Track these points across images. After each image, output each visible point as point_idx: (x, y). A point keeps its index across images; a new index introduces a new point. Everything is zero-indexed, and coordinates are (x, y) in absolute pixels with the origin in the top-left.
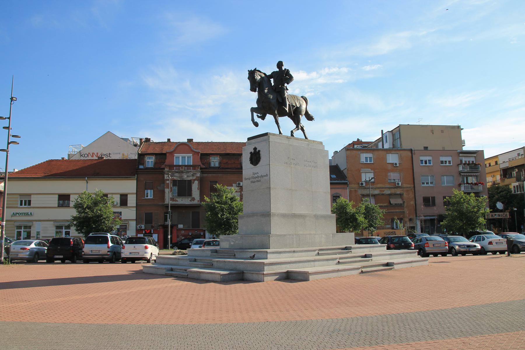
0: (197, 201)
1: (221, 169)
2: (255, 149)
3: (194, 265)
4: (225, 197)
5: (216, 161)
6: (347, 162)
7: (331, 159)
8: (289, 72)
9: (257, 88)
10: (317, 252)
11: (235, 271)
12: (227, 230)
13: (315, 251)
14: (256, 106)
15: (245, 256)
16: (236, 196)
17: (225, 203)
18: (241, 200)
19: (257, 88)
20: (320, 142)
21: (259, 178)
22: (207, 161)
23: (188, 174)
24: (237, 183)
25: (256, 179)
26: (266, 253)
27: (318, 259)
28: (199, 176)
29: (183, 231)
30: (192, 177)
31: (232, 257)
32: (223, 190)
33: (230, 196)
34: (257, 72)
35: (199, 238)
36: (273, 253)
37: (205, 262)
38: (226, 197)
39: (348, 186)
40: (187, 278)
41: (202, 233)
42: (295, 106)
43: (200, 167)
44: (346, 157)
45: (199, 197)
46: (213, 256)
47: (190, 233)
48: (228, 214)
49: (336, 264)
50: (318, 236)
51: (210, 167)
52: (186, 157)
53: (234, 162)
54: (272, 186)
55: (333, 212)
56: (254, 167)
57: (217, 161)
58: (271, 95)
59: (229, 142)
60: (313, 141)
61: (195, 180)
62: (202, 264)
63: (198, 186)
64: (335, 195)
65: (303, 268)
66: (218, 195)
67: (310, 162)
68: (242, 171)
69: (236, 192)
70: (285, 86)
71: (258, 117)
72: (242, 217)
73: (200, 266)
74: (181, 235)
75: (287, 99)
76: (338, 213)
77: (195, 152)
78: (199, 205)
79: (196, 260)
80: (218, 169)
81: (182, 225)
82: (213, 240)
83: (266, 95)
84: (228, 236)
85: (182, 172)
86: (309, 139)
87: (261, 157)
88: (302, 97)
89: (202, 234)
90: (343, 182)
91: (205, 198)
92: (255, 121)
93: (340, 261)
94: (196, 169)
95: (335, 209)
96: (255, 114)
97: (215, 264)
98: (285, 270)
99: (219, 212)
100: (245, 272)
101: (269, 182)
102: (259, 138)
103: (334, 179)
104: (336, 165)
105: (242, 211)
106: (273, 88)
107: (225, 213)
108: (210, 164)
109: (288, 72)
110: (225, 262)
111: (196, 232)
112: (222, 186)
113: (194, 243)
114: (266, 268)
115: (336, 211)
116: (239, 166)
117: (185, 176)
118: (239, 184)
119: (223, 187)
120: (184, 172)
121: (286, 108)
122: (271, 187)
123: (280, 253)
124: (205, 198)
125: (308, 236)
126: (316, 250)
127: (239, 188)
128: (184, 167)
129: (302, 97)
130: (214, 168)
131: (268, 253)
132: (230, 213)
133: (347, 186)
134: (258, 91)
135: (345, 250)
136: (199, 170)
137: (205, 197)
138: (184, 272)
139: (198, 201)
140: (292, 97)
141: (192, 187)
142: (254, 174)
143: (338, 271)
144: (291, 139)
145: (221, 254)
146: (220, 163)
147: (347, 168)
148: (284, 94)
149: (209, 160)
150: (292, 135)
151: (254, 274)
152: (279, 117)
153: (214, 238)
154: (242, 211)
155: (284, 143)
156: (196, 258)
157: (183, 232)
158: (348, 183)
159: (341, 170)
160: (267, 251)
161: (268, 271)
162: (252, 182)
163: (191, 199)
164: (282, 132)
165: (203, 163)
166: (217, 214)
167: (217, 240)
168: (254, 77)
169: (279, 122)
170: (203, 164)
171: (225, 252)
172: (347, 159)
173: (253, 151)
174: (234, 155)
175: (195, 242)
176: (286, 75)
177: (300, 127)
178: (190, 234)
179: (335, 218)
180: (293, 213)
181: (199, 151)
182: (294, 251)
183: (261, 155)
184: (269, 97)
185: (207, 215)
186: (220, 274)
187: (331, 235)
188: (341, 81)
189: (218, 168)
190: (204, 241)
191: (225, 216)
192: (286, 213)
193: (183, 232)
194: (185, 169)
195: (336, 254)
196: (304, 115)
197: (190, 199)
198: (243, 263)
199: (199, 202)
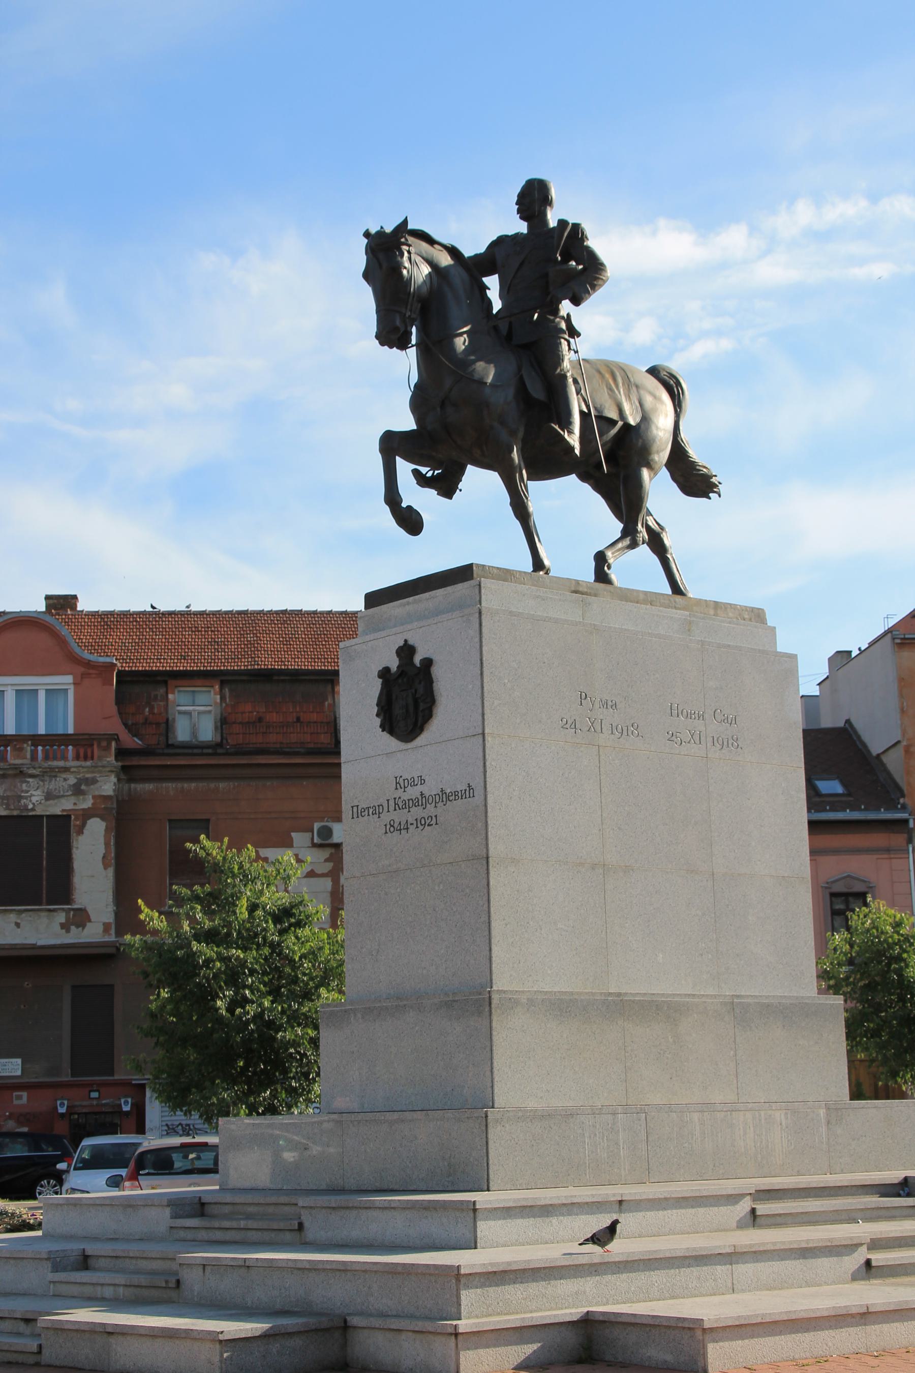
0: (101, 928)
1: (227, 754)
2: (406, 651)
3: (75, 1290)
4: (244, 903)
5: (199, 713)
6: (903, 711)
7: (816, 691)
8: (584, 238)
9: (414, 330)
10: (746, 1205)
11: (301, 1320)
12: (267, 1080)
13: (733, 1199)
14: (407, 423)
15: (356, 1234)
16: (306, 897)
17: (249, 939)
18: (334, 919)
19: (414, 330)
20: (752, 609)
21: (430, 808)
22: (151, 712)
23: (53, 785)
24: (316, 826)
25: (413, 809)
26: (471, 1214)
27: (751, 1246)
28: (111, 793)
29: (25, 1094)
30: (73, 799)
31: (288, 1236)
32: (236, 871)
33: (274, 898)
34: (411, 240)
35: (111, 1129)
36: (507, 1212)
37: (138, 1272)
38: (253, 908)
39: (910, 841)
40: (37, 1364)
41: (126, 1103)
42: (613, 423)
43: (113, 744)
44: (901, 680)
45: (111, 908)
46: (182, 1234)
47: (62, 1105)
48: (263, 995)
49: (855, 1278)
50: (749, 1115)
51: (169, 746)
52: (42, 696)
53: (298, 719)
54: (496, 849)
55: (832, 982)
56: (402, 746)
57: (210, 712)
58: (488, 362)
59: (270, 612)
60: (716, 604)
61: (87, 815)
62: (120, 1279)
63: (107, 844)
64: (839, 888)
65: (673, 1298)
66: (214, 896)
67: (701, 717)
68: (339, 765)
69: (311, 874)
70: (563, 312)
71: (422, 480)
72: (341, 1015)
73: (108, 1292)
74: (10, 1117)
75: (575, 381)
76: (861, 984)
77: (88, 664)
78: (112, 950)
79: (92, 1262)
80: (215, 754)
81: (19, 1061)
82: (184, 1146)
83: (462, 364)
84: (268, 1119)
85: (20, 774)
86: (690, 595)
87: (435, 694)
88: (653, 371)
89: (126, 1108)
90: (884, 815)
91: (141, 912)
92: (404, 505)
93: (878, 1258)
94: (92, 758)
95: (840, 965)
96: (404, 468)
97: (193, 1280)
98: (573, 1312)
99: (221, 988)
100: (354, 1321)
101: (480, 825)
102: (427, 595)
103: (835, 803)
104: (841, 724)
105: (342, 983)
106: (496, 328)
107: (252, 992)
108: (168, 726)
109: (576, 234)
110: (246, 1266)
111: (95, 1095)
112: (229, 847)
113: (83, 1161)
114: (468, 1297)
115: (847, 978)
116: (325, 739)
117: (36, 796)
118: (326, 832)
119: (239, 851)
120: (31, 771)
121: (571, 432)
122: (492, 852)
123: (546, 1211)
124: (141, 912)
125: (696, 1116)
126: (743, 1196)
127: (326, 853)
128: (28, 748)
129: (653, 371)
130: (193, 748)
131: (479, 1215)
132: (275, 993)
133: (906, 835)
134: (417, 345)
135: (899, 1196)
136: (112, 759)
137: (143, 907)
138: (19, 1334)
139: (106, 927)
140: (599, 372)
141: (74, 850)
142: (400, 784)
143: (866, 1317)
144: (595, 595)
145: (227, 1224)
146: (223, 723)
147: (904, 743)
148: (559, 360)
149: (167, 705)
150: (602, 576)
151: (403, 1336)
152: (528, 479)
153: (187, 1131)
154: (340, 976)
155: (556, 621)
156: (91, 1249)
157: (22, 1099)
158: (911, 824)
159: (869, 751)
160: (474, 1202)
161: (477, 1317)
162: (393, 828)
163: (67, 918)
164: (547, 562)
165: (130, 722)
166: (206, 996)
167: (205, 1144)
168: (396, 268)
169: (531, 509)
170: (133, 729)
171: (251, 1209)
172: (901, 695)
173: (394, 664)
174: (296, 676)
175: (86, 1155)
176: (567, 257)
177: (643, 534)
178: (62, 1110)
179: (843, 1015)
180: (610, 994)
181: (108, 660)
182: (621, 1202)
183: (436, 686)
184: (476, 377)
185: (153, 1006)
186: (221, 1337)
187: (822, 1112)
188: (881, 270)
189: (214, 748)
190: (137, 1145)
191: (252, 1009)
192: (572, 993)
193: (20, 1097)
194: (34, 757)
195: (850, 1217)
196: (664, 470)
197: (63, 920)
198: (345, 1271)
199: (113, 931)
